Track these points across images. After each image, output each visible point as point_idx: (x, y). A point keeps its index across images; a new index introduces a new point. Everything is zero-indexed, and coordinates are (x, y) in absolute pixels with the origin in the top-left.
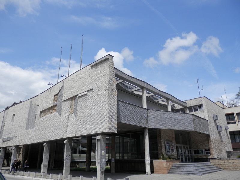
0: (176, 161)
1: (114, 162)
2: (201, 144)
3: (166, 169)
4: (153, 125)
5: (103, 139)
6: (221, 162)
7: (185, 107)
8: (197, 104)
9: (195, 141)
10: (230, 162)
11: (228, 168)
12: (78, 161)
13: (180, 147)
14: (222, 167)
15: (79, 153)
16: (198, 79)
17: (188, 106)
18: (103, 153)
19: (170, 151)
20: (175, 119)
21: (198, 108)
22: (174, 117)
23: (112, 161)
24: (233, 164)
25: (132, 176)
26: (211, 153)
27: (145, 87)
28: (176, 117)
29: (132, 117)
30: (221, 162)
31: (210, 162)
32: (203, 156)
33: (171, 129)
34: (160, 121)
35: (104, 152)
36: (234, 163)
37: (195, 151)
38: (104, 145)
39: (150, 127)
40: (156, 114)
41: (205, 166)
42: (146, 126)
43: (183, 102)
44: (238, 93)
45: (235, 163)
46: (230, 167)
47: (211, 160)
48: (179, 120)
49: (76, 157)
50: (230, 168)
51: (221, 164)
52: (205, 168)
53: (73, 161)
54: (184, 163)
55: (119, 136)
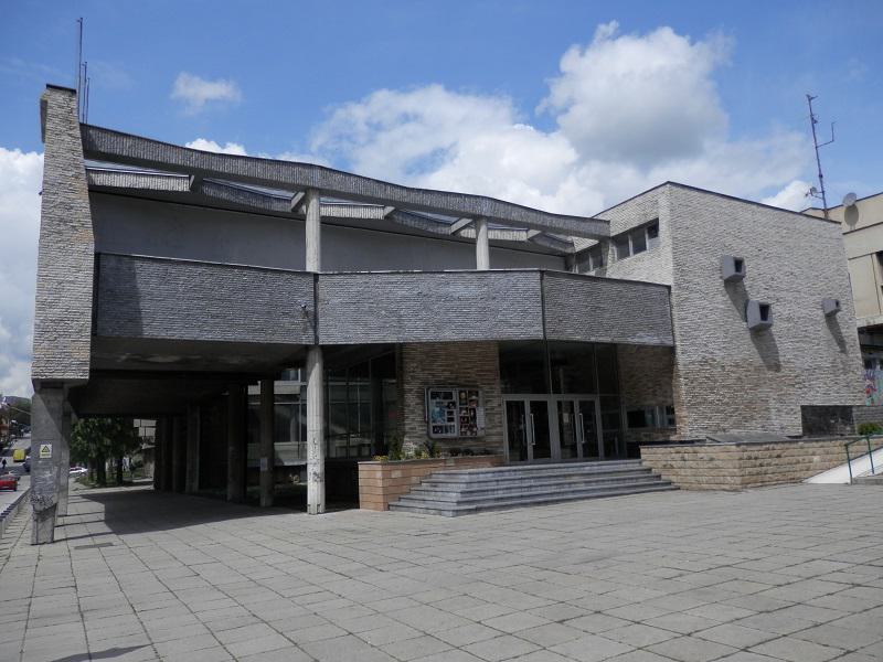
0: (457, 461)
1: (266, 469)
2: (650, 385)
3: (380, 491)
4: (339, 330)
5: (47, 403)
6: (673, 459)
7: (604, 240)
8: (643, 221)
9: (632, 376)
10: (700, 455)
11: (692, 479)
12: (296, 463)
13: (540, 409)
14: (674, 479)
15: (297, 440)
16: (810, 99)
17: (615, 231)
18: (46, 450)
19: (455, 423)
20: (448, 298)
21: (647, 236)
22: (443, 290)
23: (262, 469)
24: (710, 465)
25: (292, 515)
26: (677, 420)
27: (313, 188)
28: (451, 289)
29: (214, 311)
30: (673, 459)
31: (639, 457)
32: (655, 435)
33: (424, 339)
34: (371, 312)
35: (50, 446)
36: (712, 459)
37: (630, 414)
38: (52, 422)
39: (323, 341)
40: (354, 289)
41: (570, 475)
42: (306, 340)
43: (592, 219)
44: (41, 190)
45: (716, 462)
46: (700, 478)
47: (642, 450)
48: (467, 299)
49: (287, 452)
50: (699, 483)
51: (672, 467)
52: (550, 485)
53: (277, 464)
54: (580, 461)
55: (344, 384)
